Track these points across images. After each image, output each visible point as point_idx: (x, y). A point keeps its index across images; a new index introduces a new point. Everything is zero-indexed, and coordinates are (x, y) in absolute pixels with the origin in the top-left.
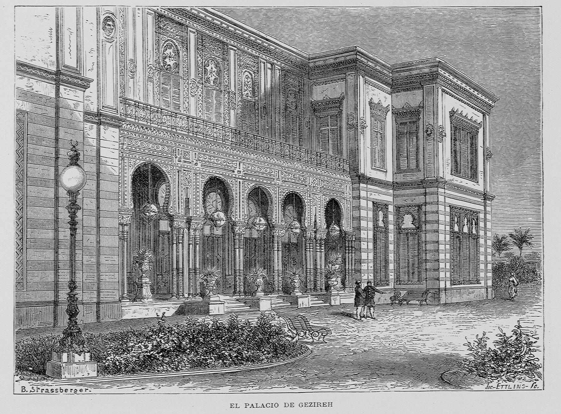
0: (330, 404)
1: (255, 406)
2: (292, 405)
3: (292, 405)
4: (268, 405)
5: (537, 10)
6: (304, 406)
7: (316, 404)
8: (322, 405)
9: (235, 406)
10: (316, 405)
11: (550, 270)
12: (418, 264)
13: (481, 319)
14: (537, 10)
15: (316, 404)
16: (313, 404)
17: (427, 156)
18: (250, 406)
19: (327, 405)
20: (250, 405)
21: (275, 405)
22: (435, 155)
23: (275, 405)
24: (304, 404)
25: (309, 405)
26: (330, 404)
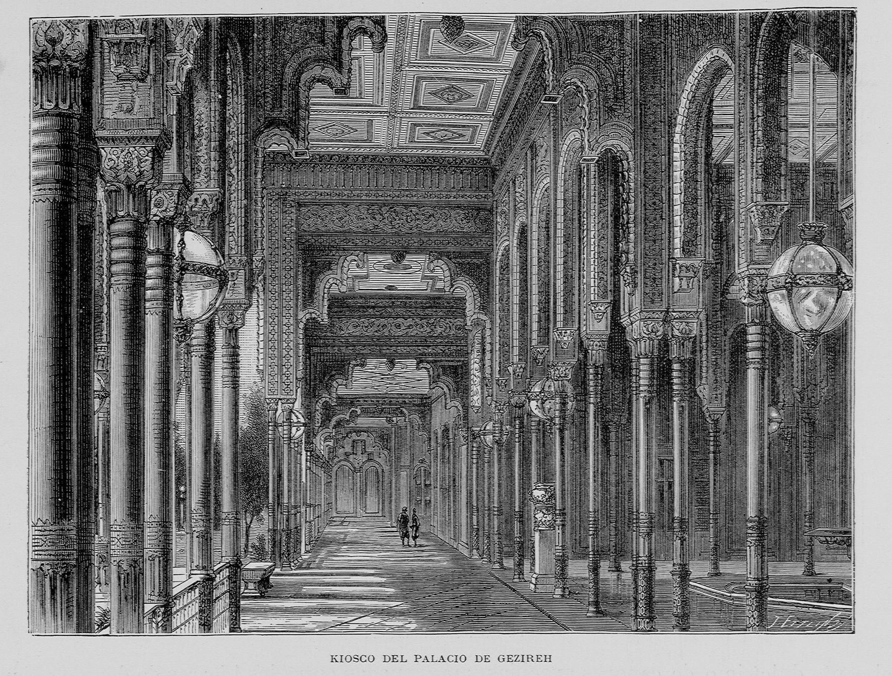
0: (548, 659)
1: (430, 659)
2: (486, 659)
3: (486, 659)
4: (451, 659)
5: (828, 603)
6: (506, 660)
7: (525, 658)
8: (535, 659)
9: (399, 659)
10: (525, 659)
11: (84, 641)
12: (846, 532)
13: (193, 138)
14: (828, 603)
15: (525, 658)
16: (520, 658)
17: (327, 137)
18: (422, 659)
19: (543, 658)
20: (423, 657)
21: (460, 659)
22: (381, 90)
23: (460, 659)
24: (506, 658)
25: (514, 659)
26: (548, 659)
